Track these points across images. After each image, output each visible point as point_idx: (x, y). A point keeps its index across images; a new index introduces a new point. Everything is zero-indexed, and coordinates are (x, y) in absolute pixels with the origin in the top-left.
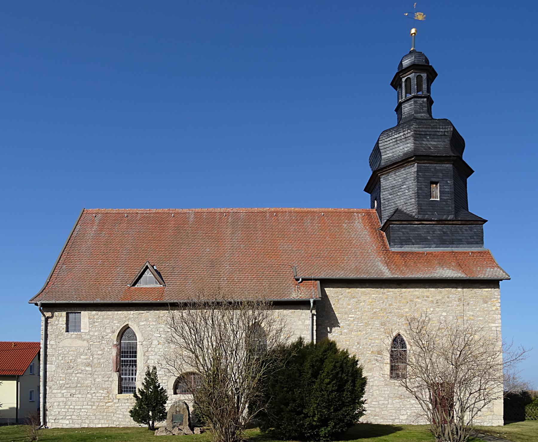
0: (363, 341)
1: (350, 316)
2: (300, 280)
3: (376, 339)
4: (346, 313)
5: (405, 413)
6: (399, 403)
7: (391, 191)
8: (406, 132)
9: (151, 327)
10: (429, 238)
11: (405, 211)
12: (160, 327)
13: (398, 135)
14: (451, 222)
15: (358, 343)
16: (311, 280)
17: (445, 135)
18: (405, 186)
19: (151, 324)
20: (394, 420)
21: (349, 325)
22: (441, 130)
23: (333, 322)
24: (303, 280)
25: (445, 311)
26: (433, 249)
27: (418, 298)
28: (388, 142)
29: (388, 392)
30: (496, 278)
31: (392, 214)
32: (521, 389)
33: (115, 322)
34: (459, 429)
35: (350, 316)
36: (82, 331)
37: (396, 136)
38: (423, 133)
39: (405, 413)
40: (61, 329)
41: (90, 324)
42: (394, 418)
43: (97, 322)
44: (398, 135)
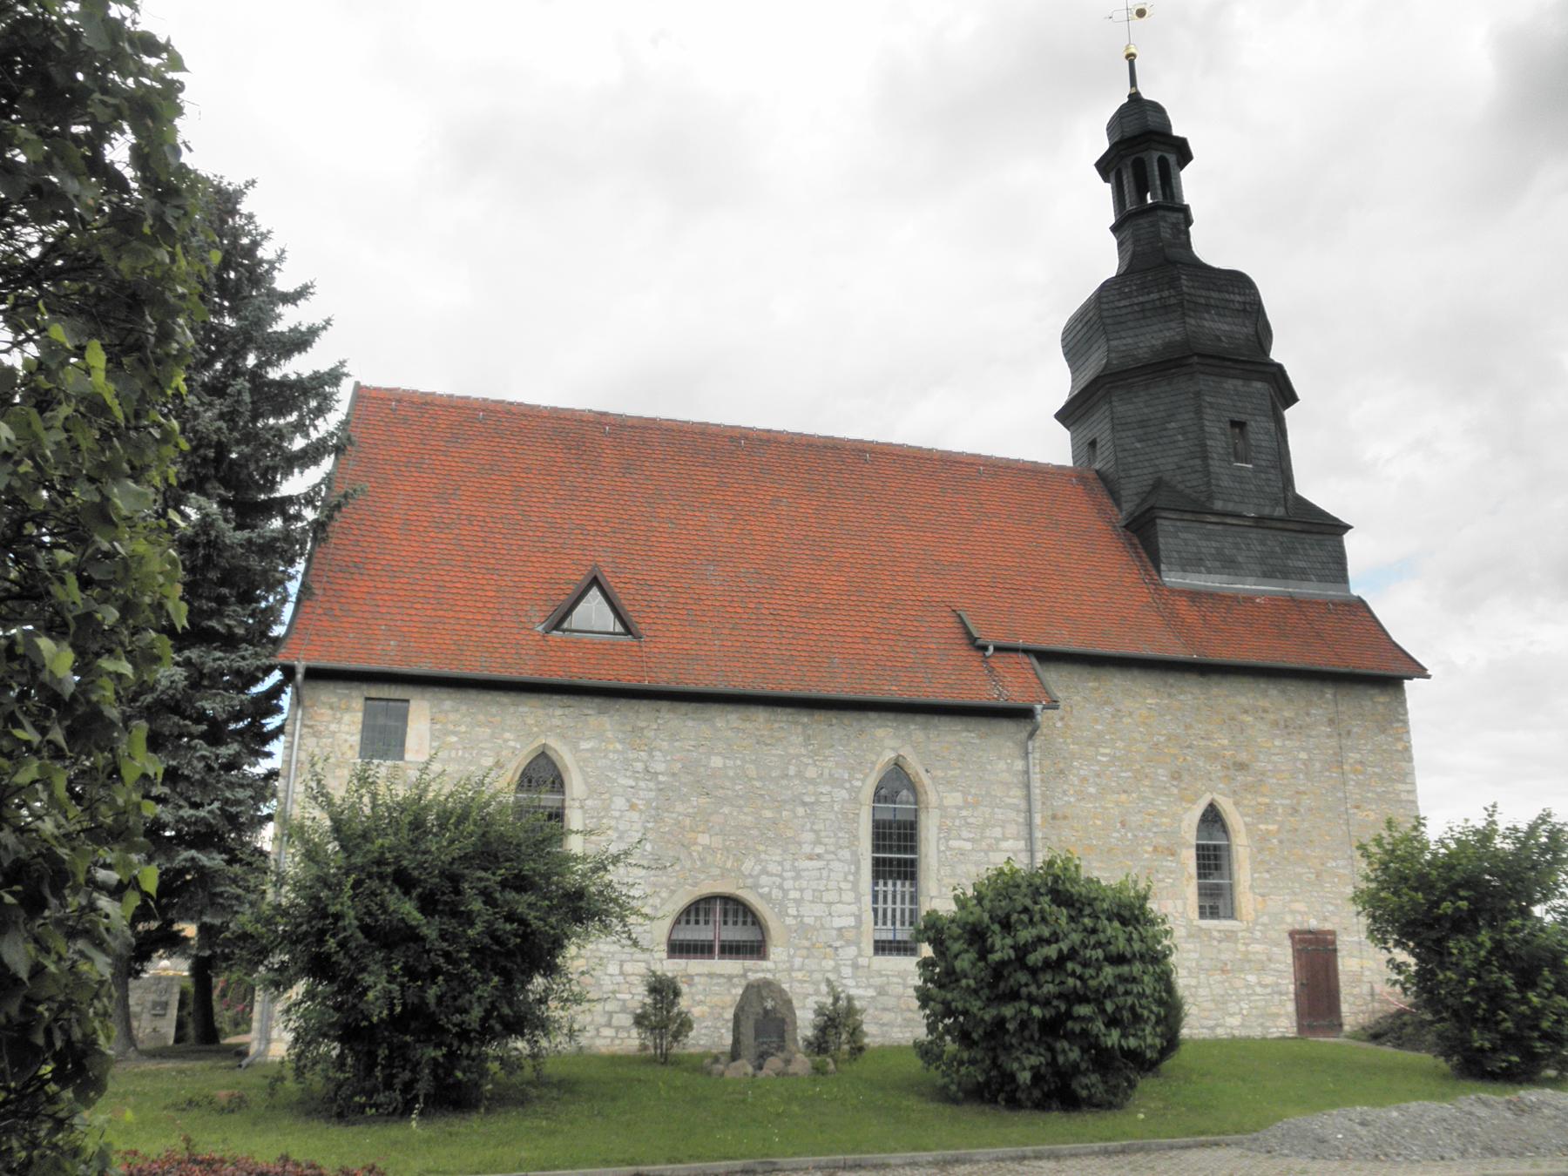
0: (1135, 819)
1: (1102, 750)
2: (991, 648)
3: (1162, 813)
4: (1090, 744)
5: (1237, 1010)
6: (1222, 982)
7: (1140, 431)
8: (1166, 294)
9: (611, 756)
10: (1240, 559)
11: (1180, 487)
12: (637, 760)
13: (1145, 298)
14: (1279, 525)
15: (1123, 824)
16: (1015, 650)
17: (1244, 310)
18: (1173, 425)
19: (611, 747)
20: (1212, 1028)
21: (1098, 776)
22: (1238, 298)
23: (1062, 765)
24: (997, 649)
25: (1304, 749)
26: (1248, 586)
27: (1246, 712)
28: (1124, 311)
29: (1196, 956)
30: (1396, 673)
31: (1147, 489)
32: (909, 734)
33: (507, 735)
34: (1125, 969)
35: (1102, 750)
36: (408, 757)
37: (1141, 299)
38: (1203, 301)
39: (1237, 1010)
40: (345, 747)
41: (433, 737)
42: (1212, 1023)
43: (454, 733)
44: (1145, 298)
